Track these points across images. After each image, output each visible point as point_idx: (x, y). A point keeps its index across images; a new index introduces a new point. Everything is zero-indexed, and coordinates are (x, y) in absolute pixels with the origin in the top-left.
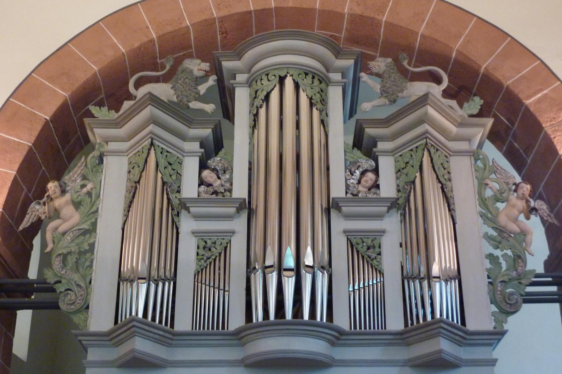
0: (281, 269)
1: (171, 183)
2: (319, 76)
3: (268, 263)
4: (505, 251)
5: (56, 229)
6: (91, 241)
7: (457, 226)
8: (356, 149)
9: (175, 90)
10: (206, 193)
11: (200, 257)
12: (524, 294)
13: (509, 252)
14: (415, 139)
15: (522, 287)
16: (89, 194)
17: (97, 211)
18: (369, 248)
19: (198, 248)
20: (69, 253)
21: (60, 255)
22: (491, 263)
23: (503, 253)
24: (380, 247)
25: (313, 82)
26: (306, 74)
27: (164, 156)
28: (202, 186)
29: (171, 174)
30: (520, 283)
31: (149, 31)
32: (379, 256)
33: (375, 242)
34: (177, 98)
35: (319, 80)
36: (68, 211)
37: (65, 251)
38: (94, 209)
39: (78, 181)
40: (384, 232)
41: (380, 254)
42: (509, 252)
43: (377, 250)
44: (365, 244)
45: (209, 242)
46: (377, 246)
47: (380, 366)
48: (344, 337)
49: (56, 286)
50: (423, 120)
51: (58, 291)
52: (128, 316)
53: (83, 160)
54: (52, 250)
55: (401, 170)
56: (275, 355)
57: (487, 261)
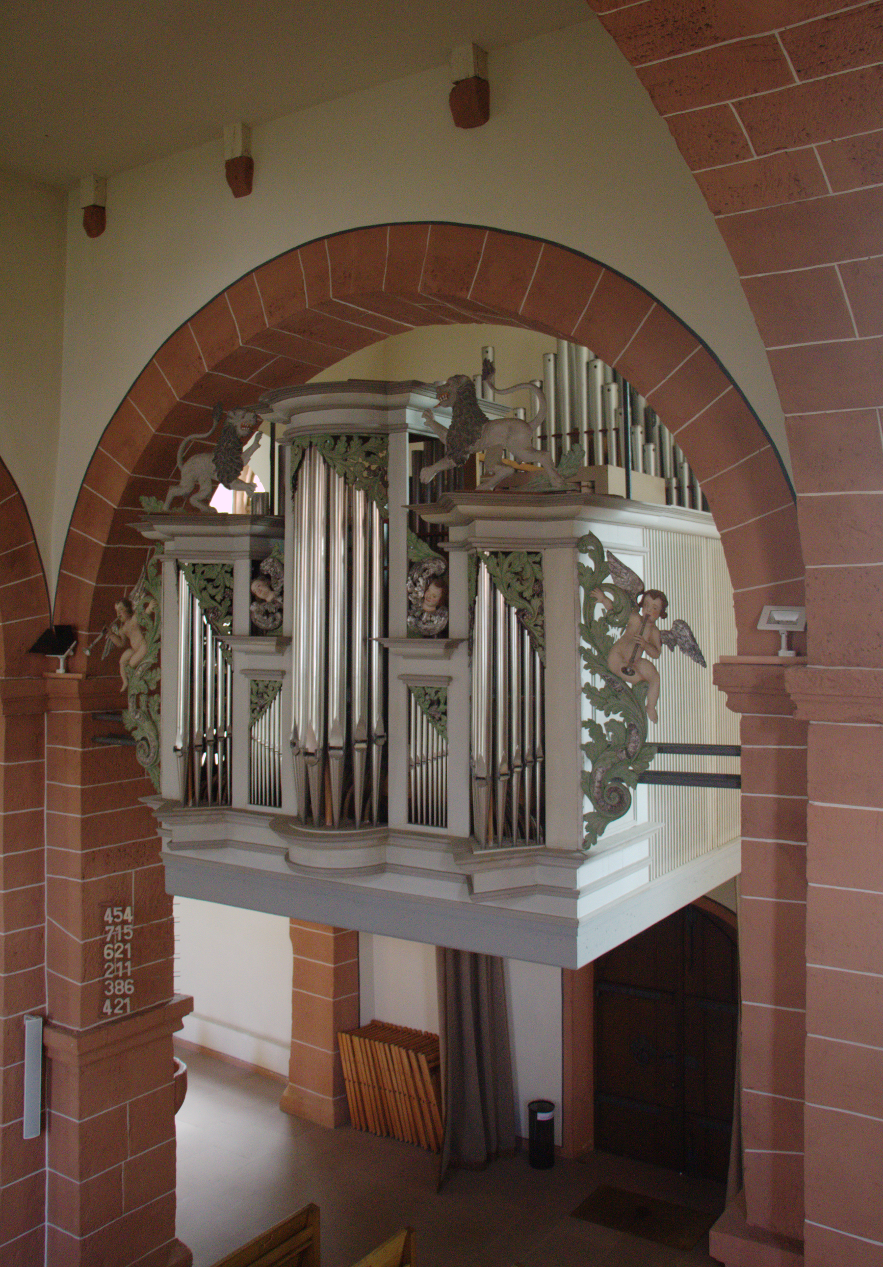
4: (612, 716)
5: (129, 661)
6: (157, 679)
7: (546, 671)
8: (420, 540)
9: (216, 464)
10: (258, 612)
11: (254, 706)
13: (618, 717)
16: (152, 616)
17: (159, 640)
19: (252, 693)
20: (140, 694)
21: (133, 695)
22: (591, 735)
23: (608, 719)
24: (445, 703)
27: (199, 574)
28: (255, 604)
31: (201, 364)
32: (443, 717)
33: (439, 694)
34: (218, 475)
36: (136, 639)
37: (136, 692)
38: (157, 637)
39: (142, 597)
41: (445, 713)
43: (442, 707)
44: (427, 697)
45: (261, 686)
46: (442, 701)
49: (134, 733)
51: (408, 510)
53: (143, 569)
54: (127, 689)
55: (500, 555)
56: (348, 832)
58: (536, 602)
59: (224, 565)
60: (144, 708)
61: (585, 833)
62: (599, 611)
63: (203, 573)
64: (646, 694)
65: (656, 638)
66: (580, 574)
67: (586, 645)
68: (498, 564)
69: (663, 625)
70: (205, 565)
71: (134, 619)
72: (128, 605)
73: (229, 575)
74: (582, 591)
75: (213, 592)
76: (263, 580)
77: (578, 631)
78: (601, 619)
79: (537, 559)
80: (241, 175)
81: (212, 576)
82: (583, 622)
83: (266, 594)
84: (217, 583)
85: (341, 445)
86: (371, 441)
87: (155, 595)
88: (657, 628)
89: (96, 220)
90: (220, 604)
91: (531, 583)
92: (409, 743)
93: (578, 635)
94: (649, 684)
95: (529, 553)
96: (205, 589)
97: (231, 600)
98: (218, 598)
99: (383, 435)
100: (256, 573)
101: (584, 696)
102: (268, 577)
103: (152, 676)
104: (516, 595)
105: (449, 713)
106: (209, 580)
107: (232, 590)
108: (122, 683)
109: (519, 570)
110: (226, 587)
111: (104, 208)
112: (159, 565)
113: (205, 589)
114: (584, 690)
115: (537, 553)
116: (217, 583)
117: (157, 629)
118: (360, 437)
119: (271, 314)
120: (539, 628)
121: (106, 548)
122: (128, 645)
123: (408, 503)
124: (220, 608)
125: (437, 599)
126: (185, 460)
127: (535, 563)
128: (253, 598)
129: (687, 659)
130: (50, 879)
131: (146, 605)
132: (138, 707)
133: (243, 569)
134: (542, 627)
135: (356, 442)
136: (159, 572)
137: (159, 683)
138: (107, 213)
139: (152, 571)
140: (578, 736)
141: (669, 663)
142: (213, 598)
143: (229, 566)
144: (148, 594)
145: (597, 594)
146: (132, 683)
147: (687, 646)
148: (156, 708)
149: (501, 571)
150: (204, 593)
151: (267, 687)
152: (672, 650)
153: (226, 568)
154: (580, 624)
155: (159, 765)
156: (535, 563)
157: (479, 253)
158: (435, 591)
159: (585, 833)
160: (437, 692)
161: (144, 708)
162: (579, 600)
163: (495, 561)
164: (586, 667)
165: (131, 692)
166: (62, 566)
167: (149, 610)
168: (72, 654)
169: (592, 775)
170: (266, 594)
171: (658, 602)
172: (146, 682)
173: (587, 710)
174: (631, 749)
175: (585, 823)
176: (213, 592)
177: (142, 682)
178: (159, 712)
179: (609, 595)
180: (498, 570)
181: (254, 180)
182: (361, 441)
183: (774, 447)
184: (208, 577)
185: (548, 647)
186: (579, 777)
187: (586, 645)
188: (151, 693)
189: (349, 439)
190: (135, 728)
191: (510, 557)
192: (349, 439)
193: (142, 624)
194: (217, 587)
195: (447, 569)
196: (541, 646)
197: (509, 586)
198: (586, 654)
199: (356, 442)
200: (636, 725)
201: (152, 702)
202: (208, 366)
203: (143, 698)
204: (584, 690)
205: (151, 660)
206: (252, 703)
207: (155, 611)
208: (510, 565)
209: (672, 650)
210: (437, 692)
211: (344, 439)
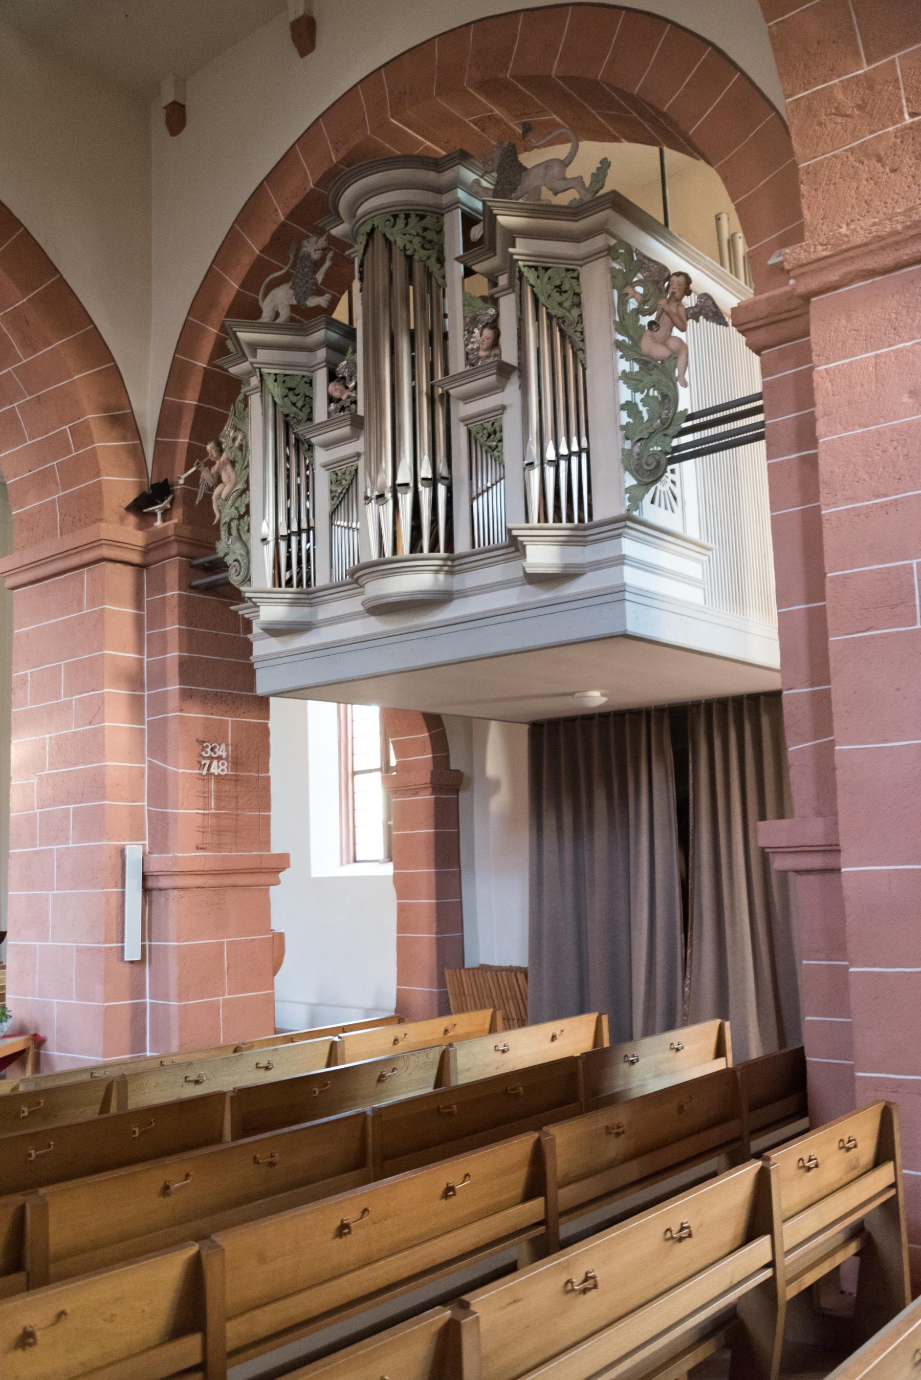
0: (432, 483)
1: (295, 413)
2: (413, 210)
3: (399, 481)
5: (220, 495)
6: (246, 502)
9: (294, 289)
11: (333, 494)
12: (670, 450)
14: (595, 254)
15: (668, 439)
16: (241, 448)
17: (248, 466)
18: (489, 436)
19: (331, 483)
20: (232, 520)
22: (629, 416)
24: (501, 431)
25: (407, 224)
26: (395, 217)
29: (294, 401)
30: (665, 435)
35: (417, 215)
37: (227, 519)
40: (503, 408)
42: (653, 393)
43: (498, 435)
46: (498, 429)
47: (485, 593)
48: (456, 563)
49: (226, 559)
50: (716, 216)
52: (356, 563)
55: (540, 269)
57: (624, 414)
58: (575, 312)
59: (303, 376)
60: (234, 533)
61: (628, 503)
62: (633, 304)
63: (284, 382)
64: (676, 366)
65: (682, 313)
66: (613, 277)
67: (620, 338)
68: (538, 277)
69: (689, 301)
70: (286, 375)
71: (224, 456)
72: (219, 444)
73: (308, 385)
74: (616, 293)
75: (294, 399)
76: (339, 381)
77: (613, 327)
78: (634, 310)
79: (575, 275)
80: (305, 34)
81: (293, 385)
82: (618, 319)
83: (342, 393)
84: (297, 392)
85: (401, 222)
86: (428, 218)
87: (242, 428)
88: (683, 306)
89: (177, 117)
90: (301, 410)
91: (570, 293)
92: (471, 479)
93: (613, 331)
94: (679, 352)
95: (567, 270)
96: (286, 396)
97: (311, 408)
98: (299, 404)
99: (439, 213)
100: (332, 376)
101: (621, 382)
102: (344, 378)
103: (244, 499)
104: (555, 304)
105: (504, 440)
106: (290, 389)
107: (311, 398)
108: (214, 516)
109: (558, 283)
110: (306, 396)
111: (184, 106)
112: (246, 400)
113: (286, 396)
114: (620, 378)
115: (574, 270)
116: (297, 392)
117: (245, 458)
118: (417, 215)
119: (337, 150)
120: (579, 334)
121: (104, 721)
122: (219, 481)
123: (461, 252)
124: (301, 414)
125: (490, 340)
126: (265, 295)
127: (572, 278)
128: (331, 400)
129: (712, 326)
130: (144, 763)
131: (234, 440)
132: (230, 534)
133: (321, 376)
134: (582, 333)
135: (413, 220)
136: (246, 406)
137: (248, 506)
138: (187, 111)
139: (240, 406)
140: (617, 418)
141: (695, 336)
142: (294, 404)
143: (308, 377)
144: (236, 429)
145: (628, 290)
146: (223, 512)
147: (710, 314)
148: (246, 528)
149: (542, 283)
150: (286, 399)
151: (344, 474)
152: (698, 321)
153: (305, 379)
154: (615, 321)
155: (250, 580)
156: (572, 278)
157: (515, 35)
158: (488, 333)
159: (628, 503)
160: (493, 424)
161: (234, 533)
162: (613, 299)
163: (536, 273)
164: (622, 357)
165: (223, 521)
166: (158, 434)
167: (237, 444)
168: (169, 506)
169: (631, 451)
170: (342, 393)
171: (681, 279)
172: (236, 508)
173: (625, 394)
174: (663, 416)
175: (628, 495)
176: (294, 399)
177: (233, 509)
178: (249, 531)
179: (640, 290)
180: (539, 281)
181: (317, 38)
182: (418, 218)
183: (778, 113)
184: (289, 386)
185: (588, 351)
186: (620, 454)
187: (620, 338)
188: (241, 517)
189: (407, 216)
190: (226, 554)
191: (549, 272)
192: (407, 216)
193: (231, 458)
194: (298, 395)
195: (498, 315)
196: (581, 350)
197: (549, 296)
198: (619, 345)
199: (413, 220)
200: (669, 398)
201: (242, 524)
202: (284, 215)
203: (234, 524)
204: (620, 378)
205: (240, 486)
206: (331, 492)
207: (244, 443)
208: (550, 279)
209: (698, 321)
210: (493, 424)
211: (402, 216)
